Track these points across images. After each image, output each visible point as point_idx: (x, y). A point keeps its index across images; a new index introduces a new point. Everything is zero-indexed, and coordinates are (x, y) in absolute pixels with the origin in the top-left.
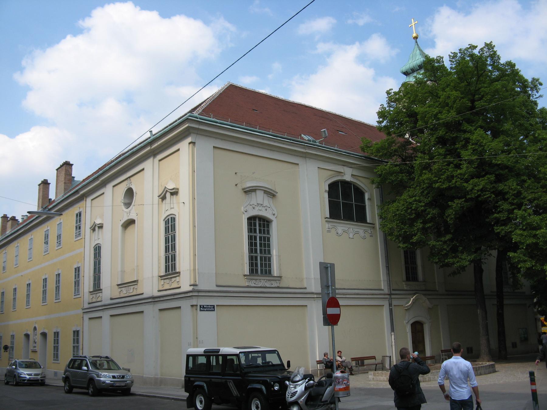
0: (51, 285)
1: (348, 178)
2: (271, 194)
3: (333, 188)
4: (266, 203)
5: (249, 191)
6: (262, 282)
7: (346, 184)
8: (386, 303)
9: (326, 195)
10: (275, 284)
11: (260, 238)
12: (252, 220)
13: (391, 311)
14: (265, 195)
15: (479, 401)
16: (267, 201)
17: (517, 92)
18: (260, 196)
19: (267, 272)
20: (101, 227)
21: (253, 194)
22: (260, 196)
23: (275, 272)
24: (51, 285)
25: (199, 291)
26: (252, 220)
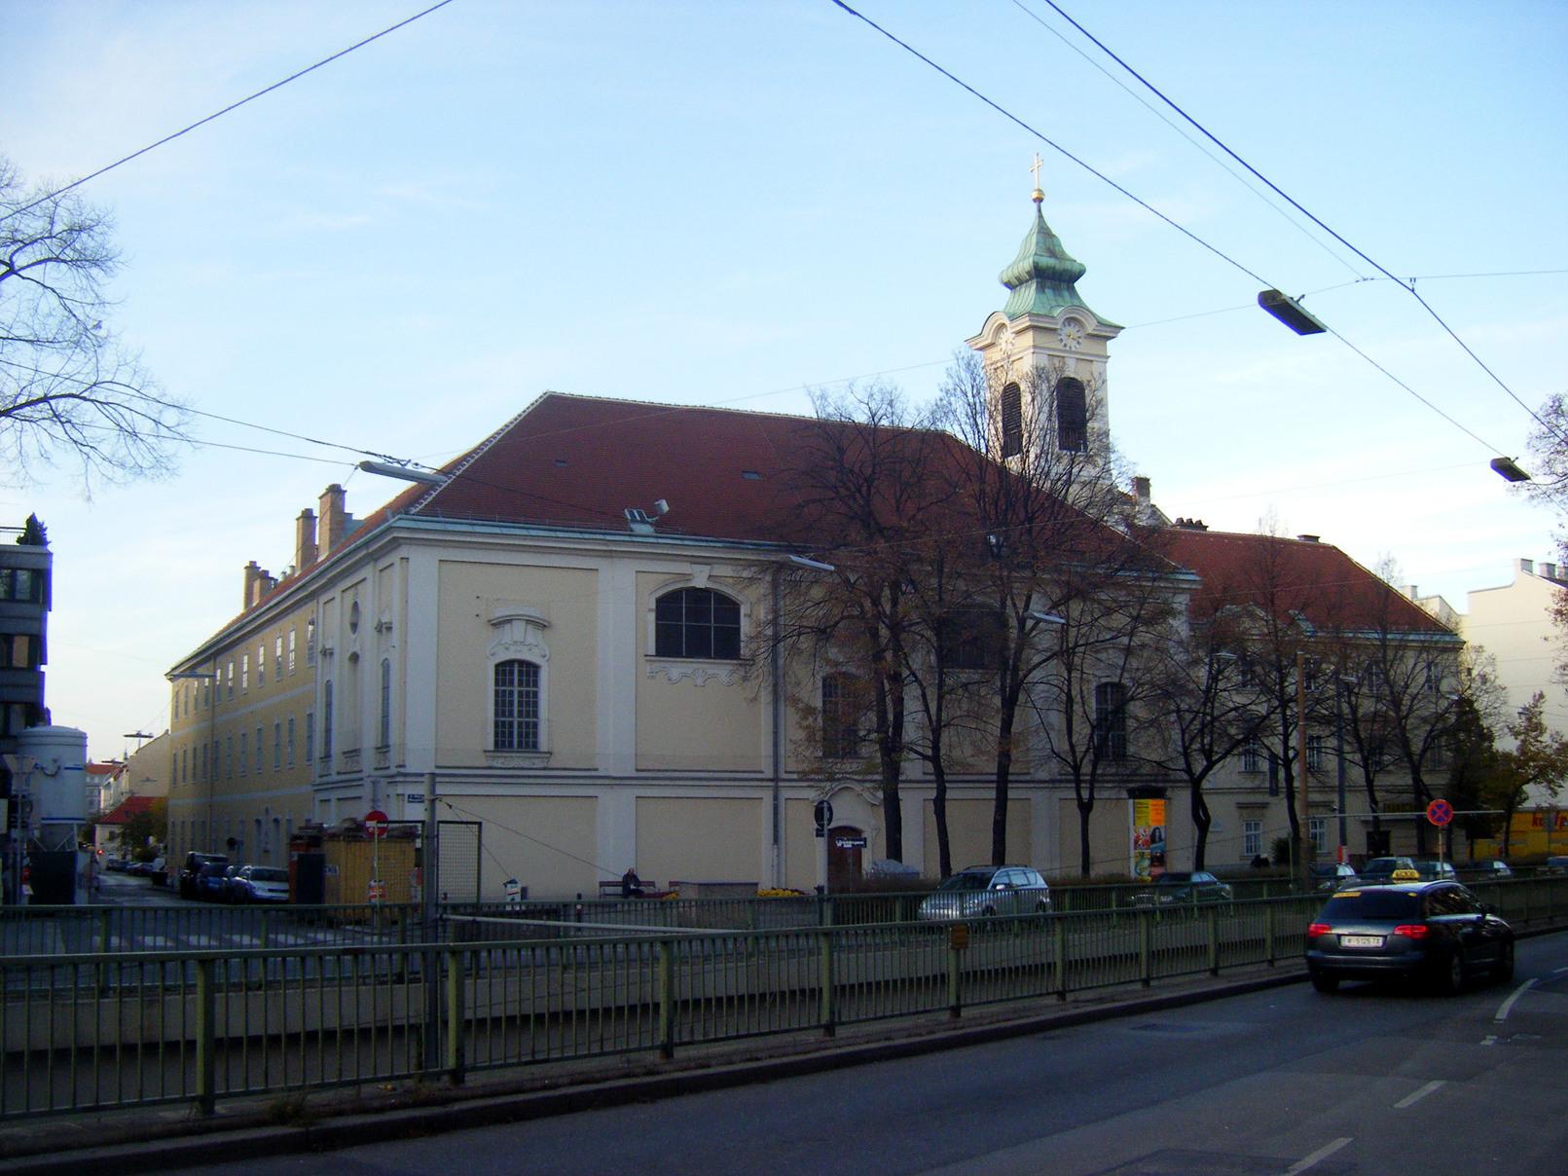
0: (285, 729)
1: (700, 579)
2: (541, 625)
3: (667, 606)
4: (530, 639)
5: (498, 624)
6: (516, 760)
7: (699, 597)
8: (767, 796)
9: (652, 616)
10: (539, 764)
11: (520, 693)
12: (504, 670)
13: (776, 808)
14: (530, 627)
15: (566, 1080)
16: (533, 636)
17: (146, 840)
18: (518, 630)
19: (528, 739)
20: (389, 629)
21: (507, 626)
22: (518, 630)
23: (544, 743)
24: (285, 729)
25: (405, 775)
26: (504, 670)
